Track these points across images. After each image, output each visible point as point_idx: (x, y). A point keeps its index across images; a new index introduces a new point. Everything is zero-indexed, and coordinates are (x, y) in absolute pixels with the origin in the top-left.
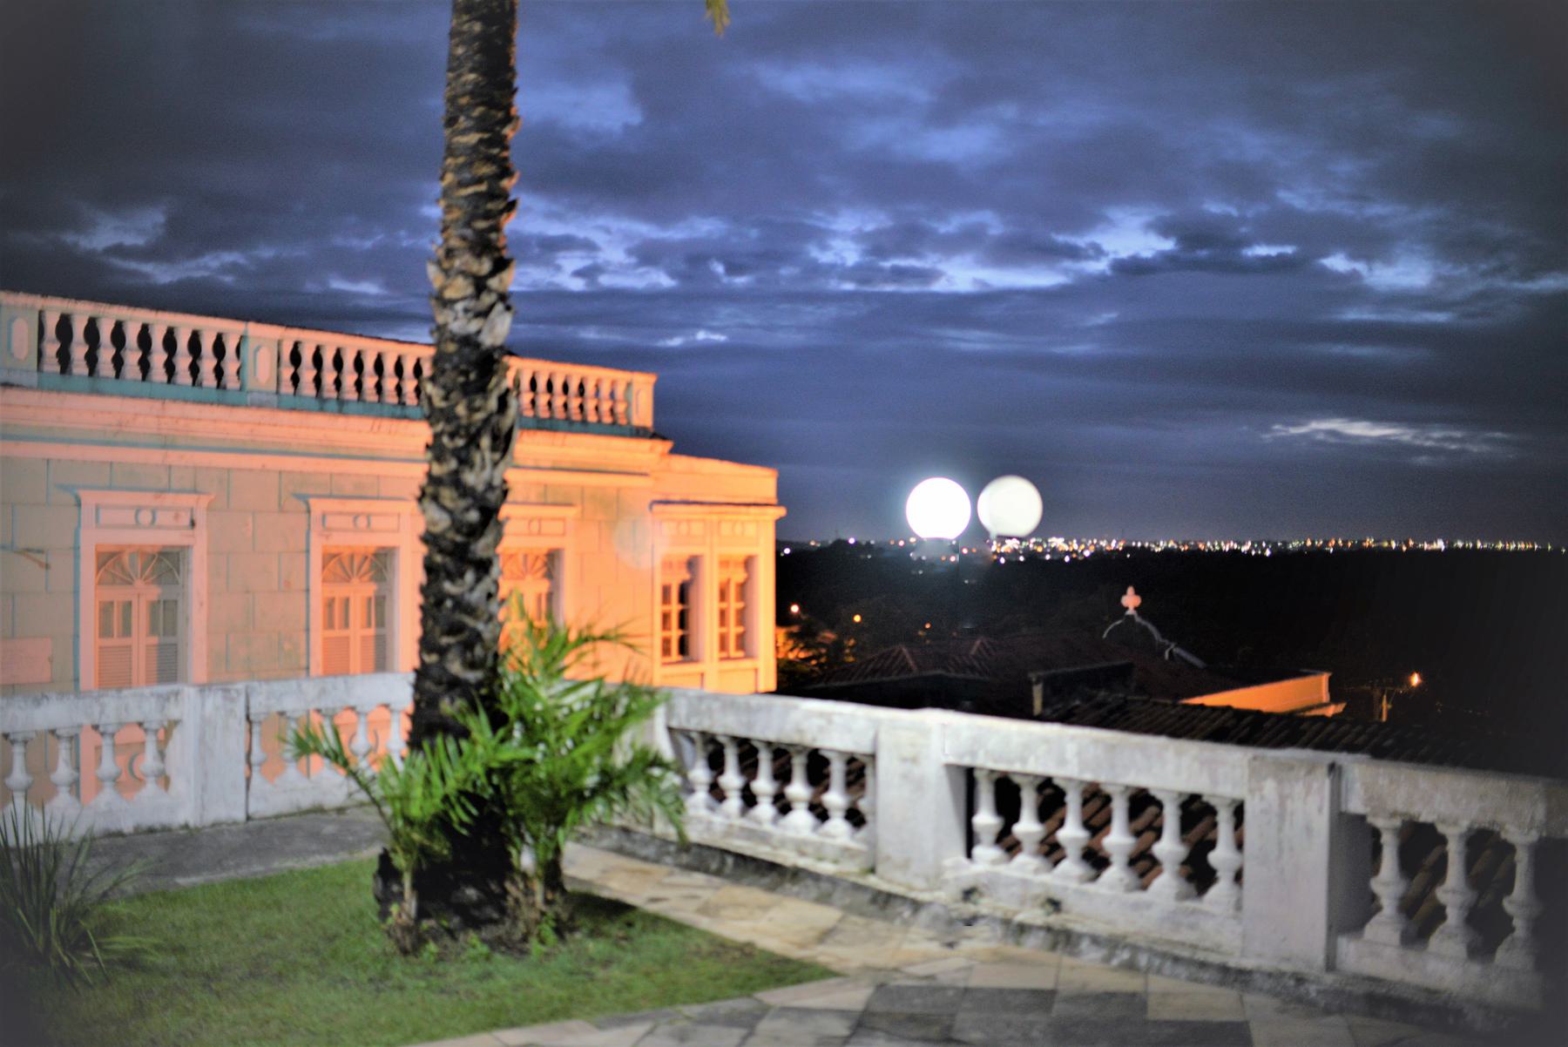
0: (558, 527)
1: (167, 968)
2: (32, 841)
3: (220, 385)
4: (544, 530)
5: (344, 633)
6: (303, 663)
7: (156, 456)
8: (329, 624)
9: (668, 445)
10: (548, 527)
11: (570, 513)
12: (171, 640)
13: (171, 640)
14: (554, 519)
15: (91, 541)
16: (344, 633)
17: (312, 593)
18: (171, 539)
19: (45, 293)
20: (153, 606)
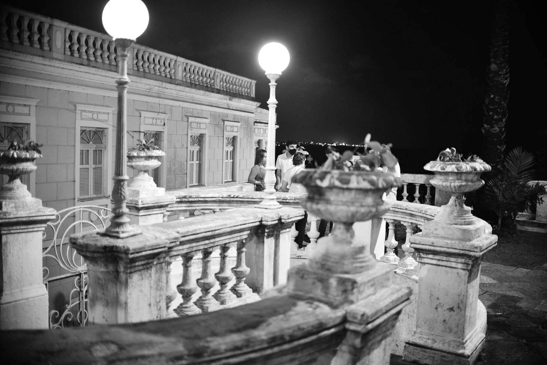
5: (87, 166)
6: (186, 173)
7: (157, 100)
8: (82, 163)
15: (80, 124)
20: (95, 151)
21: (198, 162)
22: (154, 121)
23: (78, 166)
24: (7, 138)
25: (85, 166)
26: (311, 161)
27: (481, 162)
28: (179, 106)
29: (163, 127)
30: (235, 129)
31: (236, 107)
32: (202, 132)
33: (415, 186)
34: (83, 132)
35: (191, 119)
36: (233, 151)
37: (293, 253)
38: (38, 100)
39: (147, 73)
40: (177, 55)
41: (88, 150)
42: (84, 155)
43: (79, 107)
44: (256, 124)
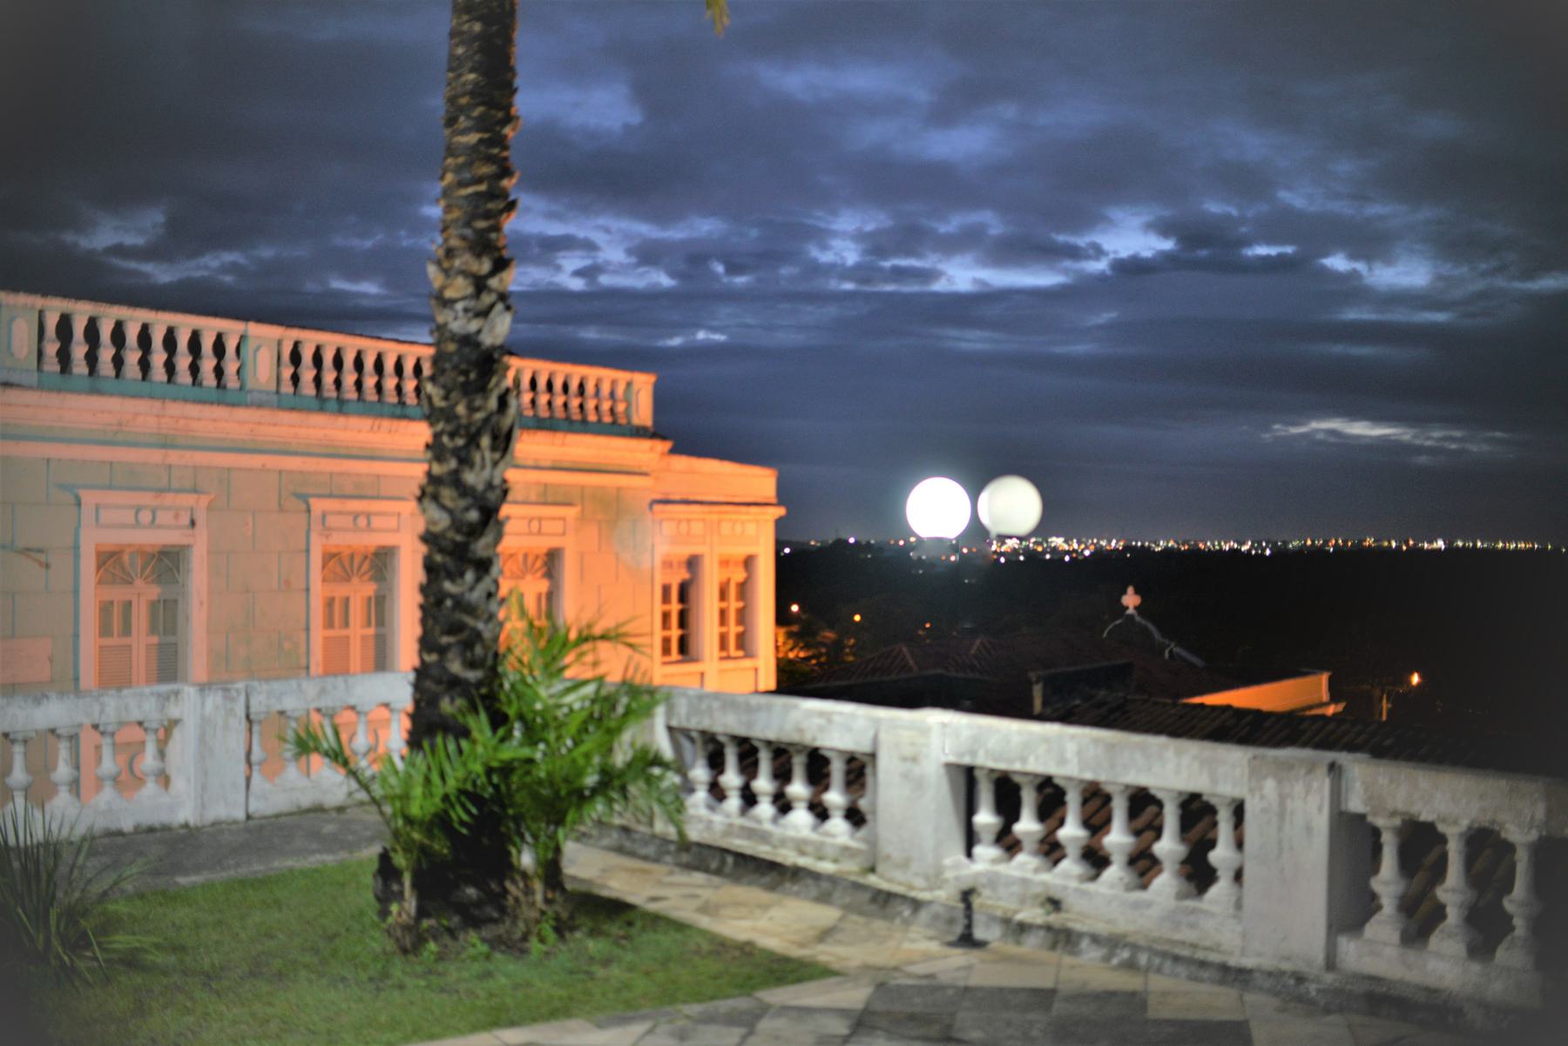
5: (344, 632)
6: (303, 662)
7: (155, 456)
8: (329, 624)
11: (571, 512)
12: (171, 639)
13: (171, 639)
15: (91, 541)
20: (153, 605)
21: (371, 631)
22: (684, 527)
23: (318, 634)
24: (141, 575)
25: (336, 632)
26: (1136, 608)
27: (897, 974)
28: (264, 469)
29: (190, 532)
30: (548, 526)
31: (536, 460)
32: (554, 542)
33: (1107, 799)
34: (328, 557)
35: (318, 506)
36: (377, 598)
37: (312, 1027)
38: (212, 497)
39: (107, 377)
40: (45, 293)
41: (130, 603)
42: (336, 612)
43: (89, 498)
44: (657, 508)
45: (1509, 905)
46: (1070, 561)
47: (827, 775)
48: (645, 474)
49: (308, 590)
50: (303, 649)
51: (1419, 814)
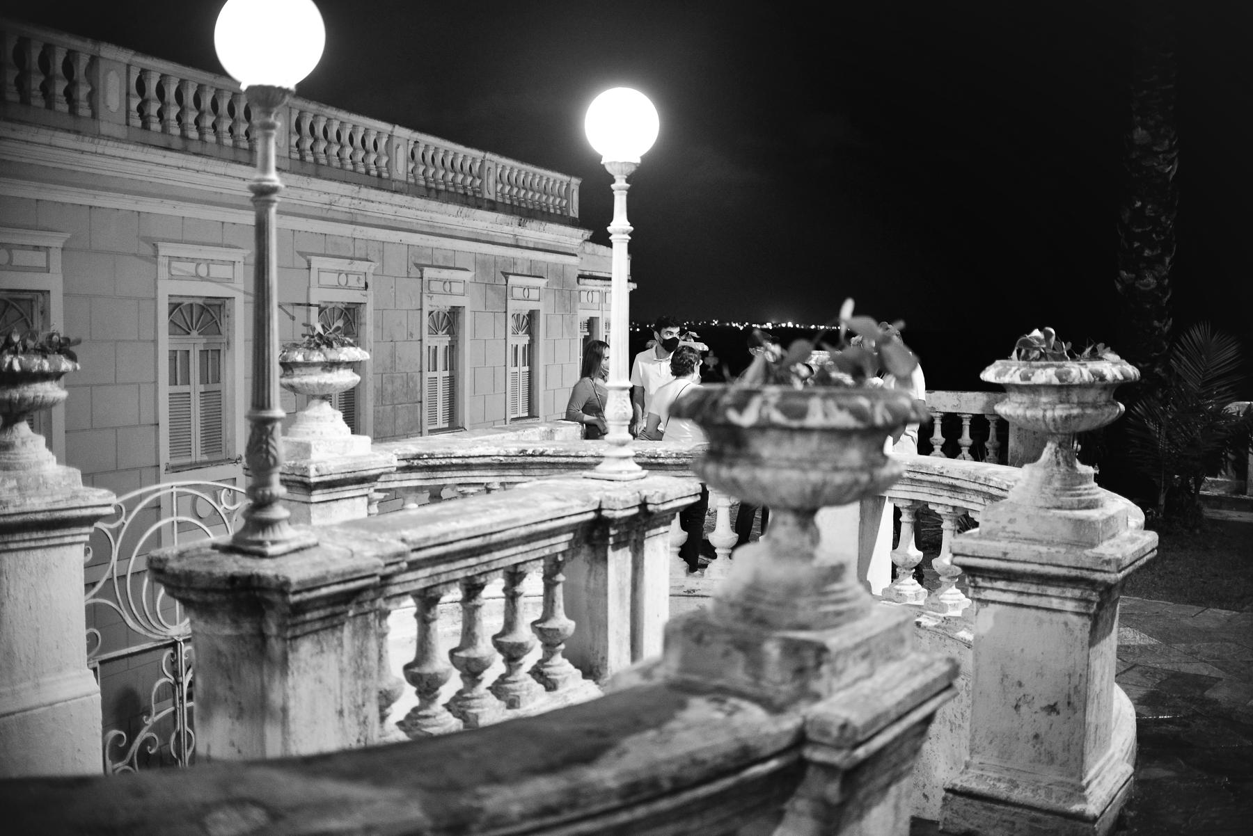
0: (225, 271)
1: (731, 507)
2: (1185, 337)
3: (73, 111)
4: (213, 274)
5: (185, 389)
6: (419, 399)
7: (347, 230)
8: (173, 382)
9: (587, 234)
10: (534, 294)
11: (541, 283)
12: (215, 387)
13: (215, 387)
14: (223, 262)
15: (168, 289)
16: (185, 389)
17: (424, 341)
18: (354, 297)
19: (393, 121)
20: (204, 353)
21: (447, 374)
23: (165, 389)
28: (401, 243)
32: (533, 306)
42: (179, 361)
43: (165, 250)
45: (987, 445)
46: (1101, 342)
47: (250, 578)
48: (575, 255)
49: (421, 340)
50: (419, 388)
51: (1051, 381)
